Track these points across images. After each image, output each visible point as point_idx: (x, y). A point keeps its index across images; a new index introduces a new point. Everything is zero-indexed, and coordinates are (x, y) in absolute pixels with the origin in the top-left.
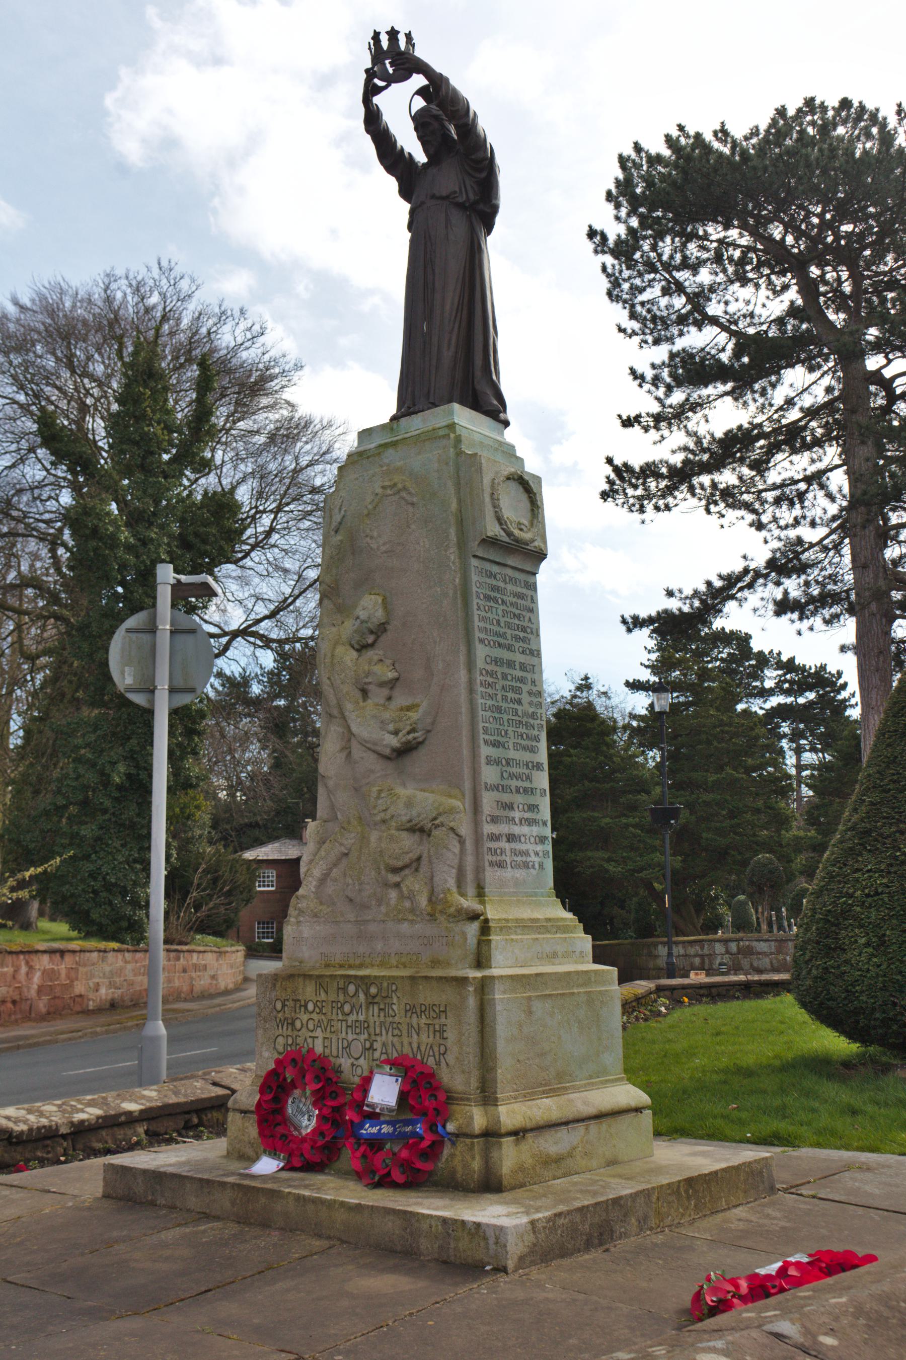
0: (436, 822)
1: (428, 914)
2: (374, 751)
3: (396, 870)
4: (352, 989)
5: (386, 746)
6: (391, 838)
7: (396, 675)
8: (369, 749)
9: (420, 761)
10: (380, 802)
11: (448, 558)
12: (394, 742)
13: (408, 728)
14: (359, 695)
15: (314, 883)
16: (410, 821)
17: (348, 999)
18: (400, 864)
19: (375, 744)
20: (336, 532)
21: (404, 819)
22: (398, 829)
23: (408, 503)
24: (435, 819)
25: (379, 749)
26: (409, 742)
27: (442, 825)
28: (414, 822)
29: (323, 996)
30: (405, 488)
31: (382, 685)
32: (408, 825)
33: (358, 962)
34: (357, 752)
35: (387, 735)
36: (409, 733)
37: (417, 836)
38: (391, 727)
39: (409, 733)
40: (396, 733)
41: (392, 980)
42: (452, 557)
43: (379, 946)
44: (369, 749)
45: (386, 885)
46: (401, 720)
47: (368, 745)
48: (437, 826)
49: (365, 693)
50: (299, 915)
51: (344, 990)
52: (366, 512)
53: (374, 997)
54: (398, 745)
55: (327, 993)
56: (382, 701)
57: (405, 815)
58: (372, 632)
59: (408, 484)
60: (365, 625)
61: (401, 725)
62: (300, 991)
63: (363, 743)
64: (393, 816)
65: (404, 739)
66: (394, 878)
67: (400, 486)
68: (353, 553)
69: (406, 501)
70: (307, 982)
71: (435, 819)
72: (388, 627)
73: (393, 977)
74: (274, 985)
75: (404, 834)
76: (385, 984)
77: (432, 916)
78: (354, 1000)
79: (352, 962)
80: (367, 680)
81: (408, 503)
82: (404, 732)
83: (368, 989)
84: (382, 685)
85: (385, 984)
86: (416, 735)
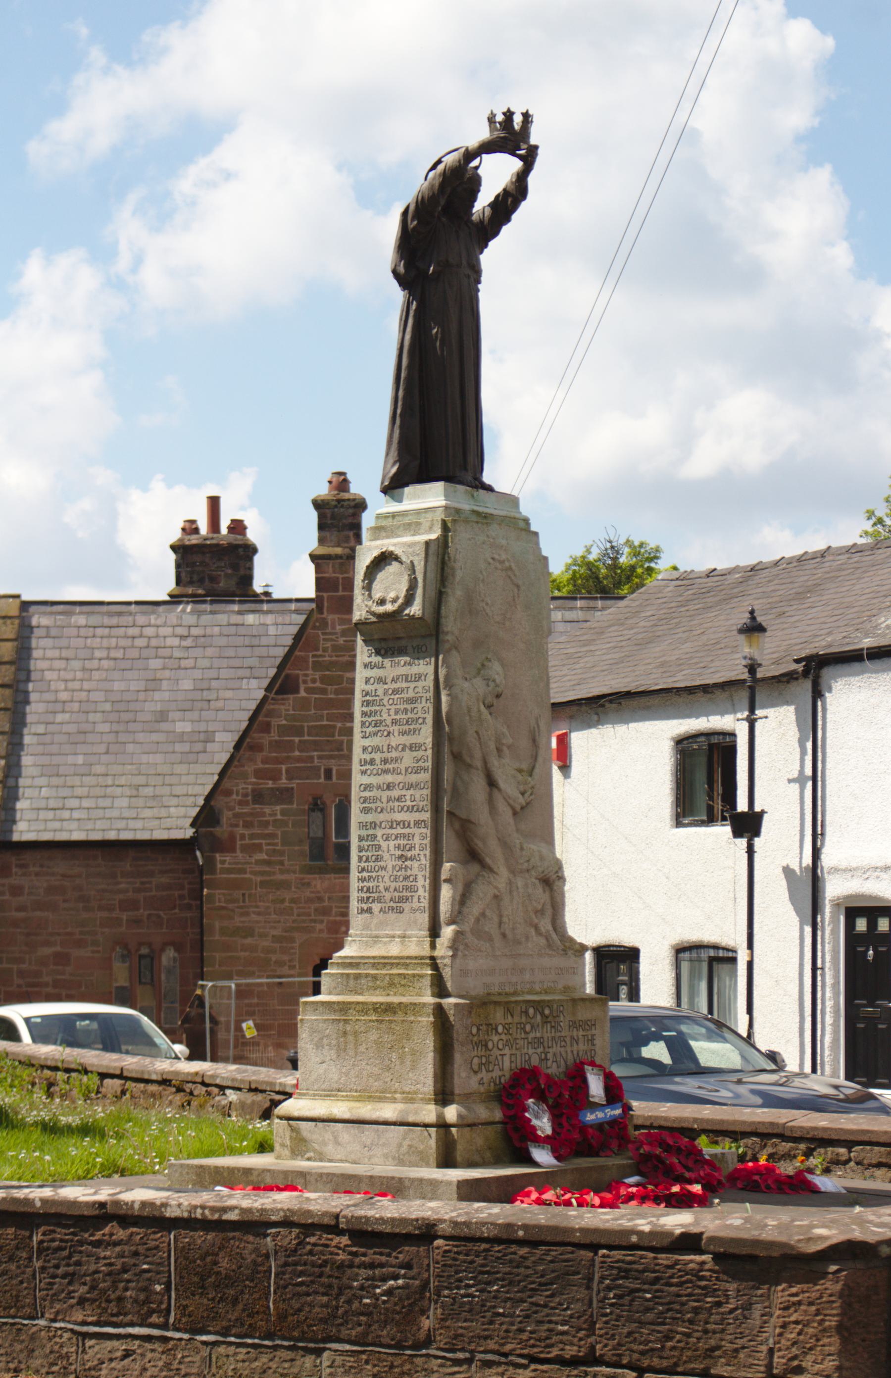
8: (509, 804)
29: (510, 1020)
30: (510, 568)
33: (512, 991)
74: (470, 1012)
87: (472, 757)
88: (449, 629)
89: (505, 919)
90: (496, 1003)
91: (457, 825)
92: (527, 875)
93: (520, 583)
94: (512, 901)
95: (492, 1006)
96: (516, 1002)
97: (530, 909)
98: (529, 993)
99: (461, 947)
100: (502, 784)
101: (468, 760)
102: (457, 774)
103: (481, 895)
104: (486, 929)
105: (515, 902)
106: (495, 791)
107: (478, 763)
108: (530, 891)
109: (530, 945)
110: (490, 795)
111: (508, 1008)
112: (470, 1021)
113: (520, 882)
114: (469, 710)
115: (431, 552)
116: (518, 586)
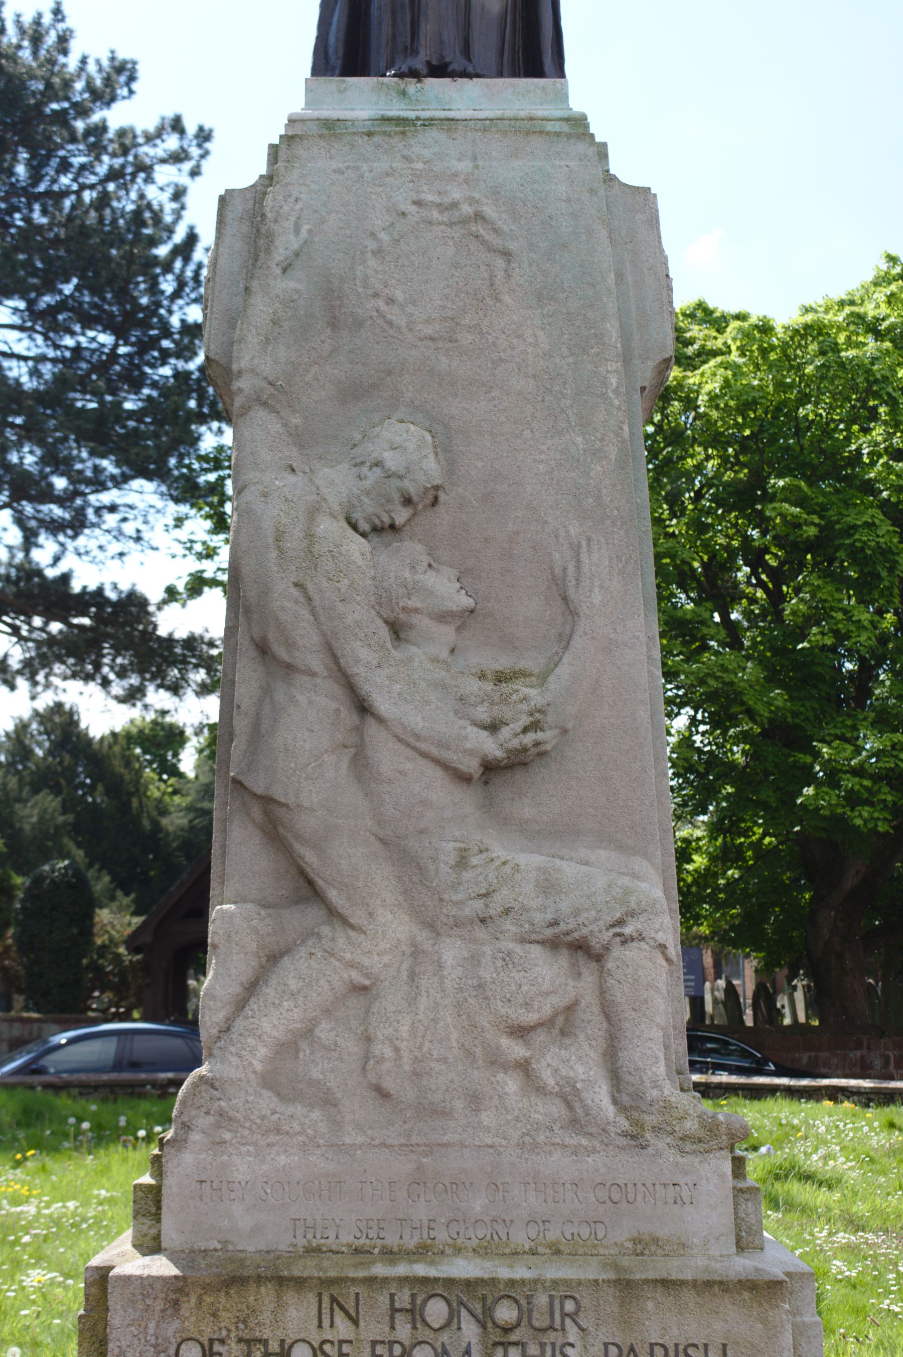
0: (628, 930)
1: (625, 1134)
2: (437, 761)
3: (520, 1032)
4: (436, 1311)
5: (471, 752)
6: (507, 958)
7: (468, 602)
8: (424, 755)
9: (533, 800)
10: (467, 875)
11: (605, 383)
12: (492, 747)
13: (525, 720)
14: (384, 632)
15: (262, 1051)
16: (555, 923)
17: (428, 1335)
18: (531, 1018)
19: (441, 744)
20: (284, 271)
21: (539, 918)
22: (523, 940)
23: (491, 249)
24: (620, 923)
25: (445, 755)
26: (525, 749)
27: (641, 938)
28: (563, 927)
29: (343, 1328)
30: (479, 217)
31: (443, 617)
32: (549, 933)
33: (411, 1243)
34: (386, 755)
35: (472, 731)
36: (525, 730)
37: (564, 959)
38: (483, 713)
39: (525, 730)
40: (493, 727)
41: (564, 1290)
42: (614, 381)
43: (478, 1204)
44: (424, 755)
45: (497, 1062)
46: (505, 699)
47: (423, 746)
48: (626, 940)
49: (397, 630)
50: (218, 1126)
51: (415, 1314)
52: (372, 245)
53: (507, 1330)
54: (499, 754)
55: (355, 1322)
56: (444, 654)
57: (543, 909)
58: (408, 501)
59: (489, 210)
60: (397, 483)
61: (506, 712)
62: (266, 1317)
63: (409, 741)
64: (507, 911)
65: (515, 743)
66: (516, 1050)
67: (467, 209)
68: (334, 324)
69: (484, 242)
70: (290, 1296)
71: (620, 923)
72: (442, 497)
73: (567, 1283)
74: (176, 1304)
75: (536, 951)
76: (542, 1300)
77: (635, 1138)
78: (445, 1337)
79: (392, 1240)
80: (410, 604)
81: (491, 249)
82: (518, 726)
83: (488, 1311)
84: (443, 617)
85: (542, 1300)
86: (540, 736)
87: (290, 645)
88: (244, 364)
89: (382, 1049)
90: (300, 1283)
91: (256, 812)
92: (480, 933)
93: (512, 246)
94: (412, 1000)
95: (267, 1292)
96: (371, 1281)
97: (484, 1021)
98: (483, 1251)
99: (203, 1121)
100: (383, 705)
101: (282, 653)
102: (266, 692)
103: (293, 984)
104: (316, 1074)
105: (424, 1002)
106: (372, 728)
107: (316, 662)
108: (487, 974)
109: (487, 1118)
110: (359, 730)
111: (334, 1295)
112: (171, 1329)
113: (451, 952)
114: (279, 536)
115: (229, 216)
116: (507, 254)
